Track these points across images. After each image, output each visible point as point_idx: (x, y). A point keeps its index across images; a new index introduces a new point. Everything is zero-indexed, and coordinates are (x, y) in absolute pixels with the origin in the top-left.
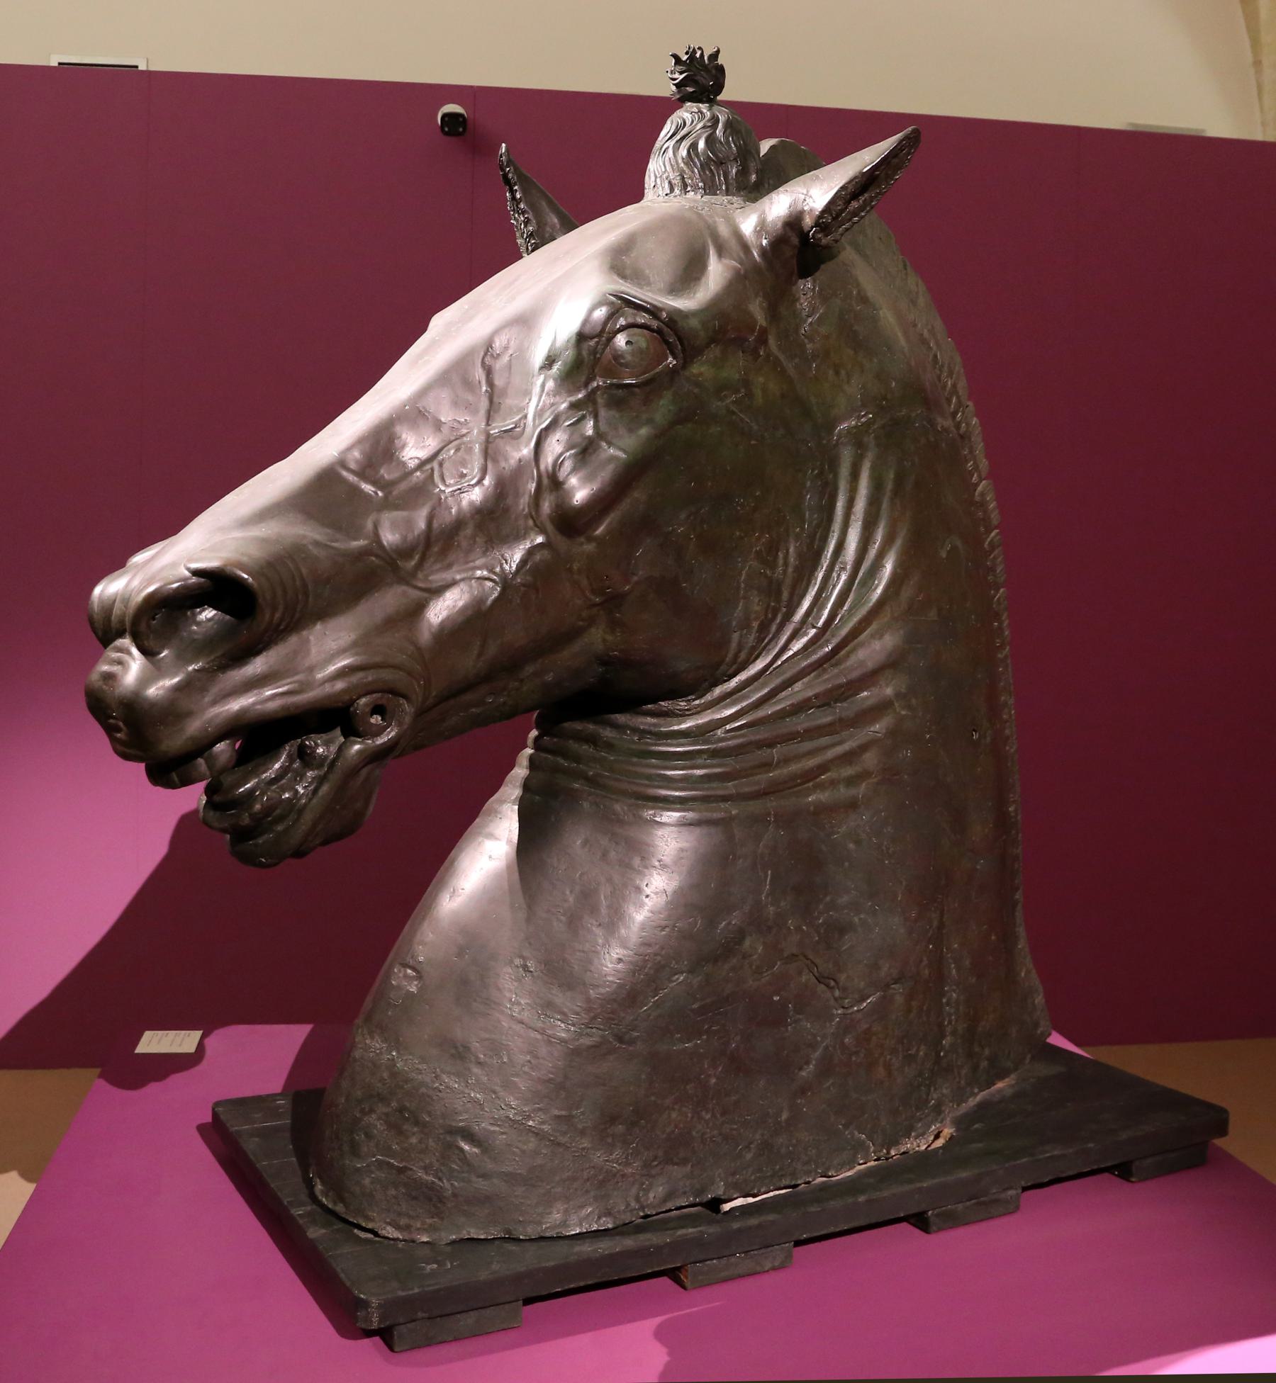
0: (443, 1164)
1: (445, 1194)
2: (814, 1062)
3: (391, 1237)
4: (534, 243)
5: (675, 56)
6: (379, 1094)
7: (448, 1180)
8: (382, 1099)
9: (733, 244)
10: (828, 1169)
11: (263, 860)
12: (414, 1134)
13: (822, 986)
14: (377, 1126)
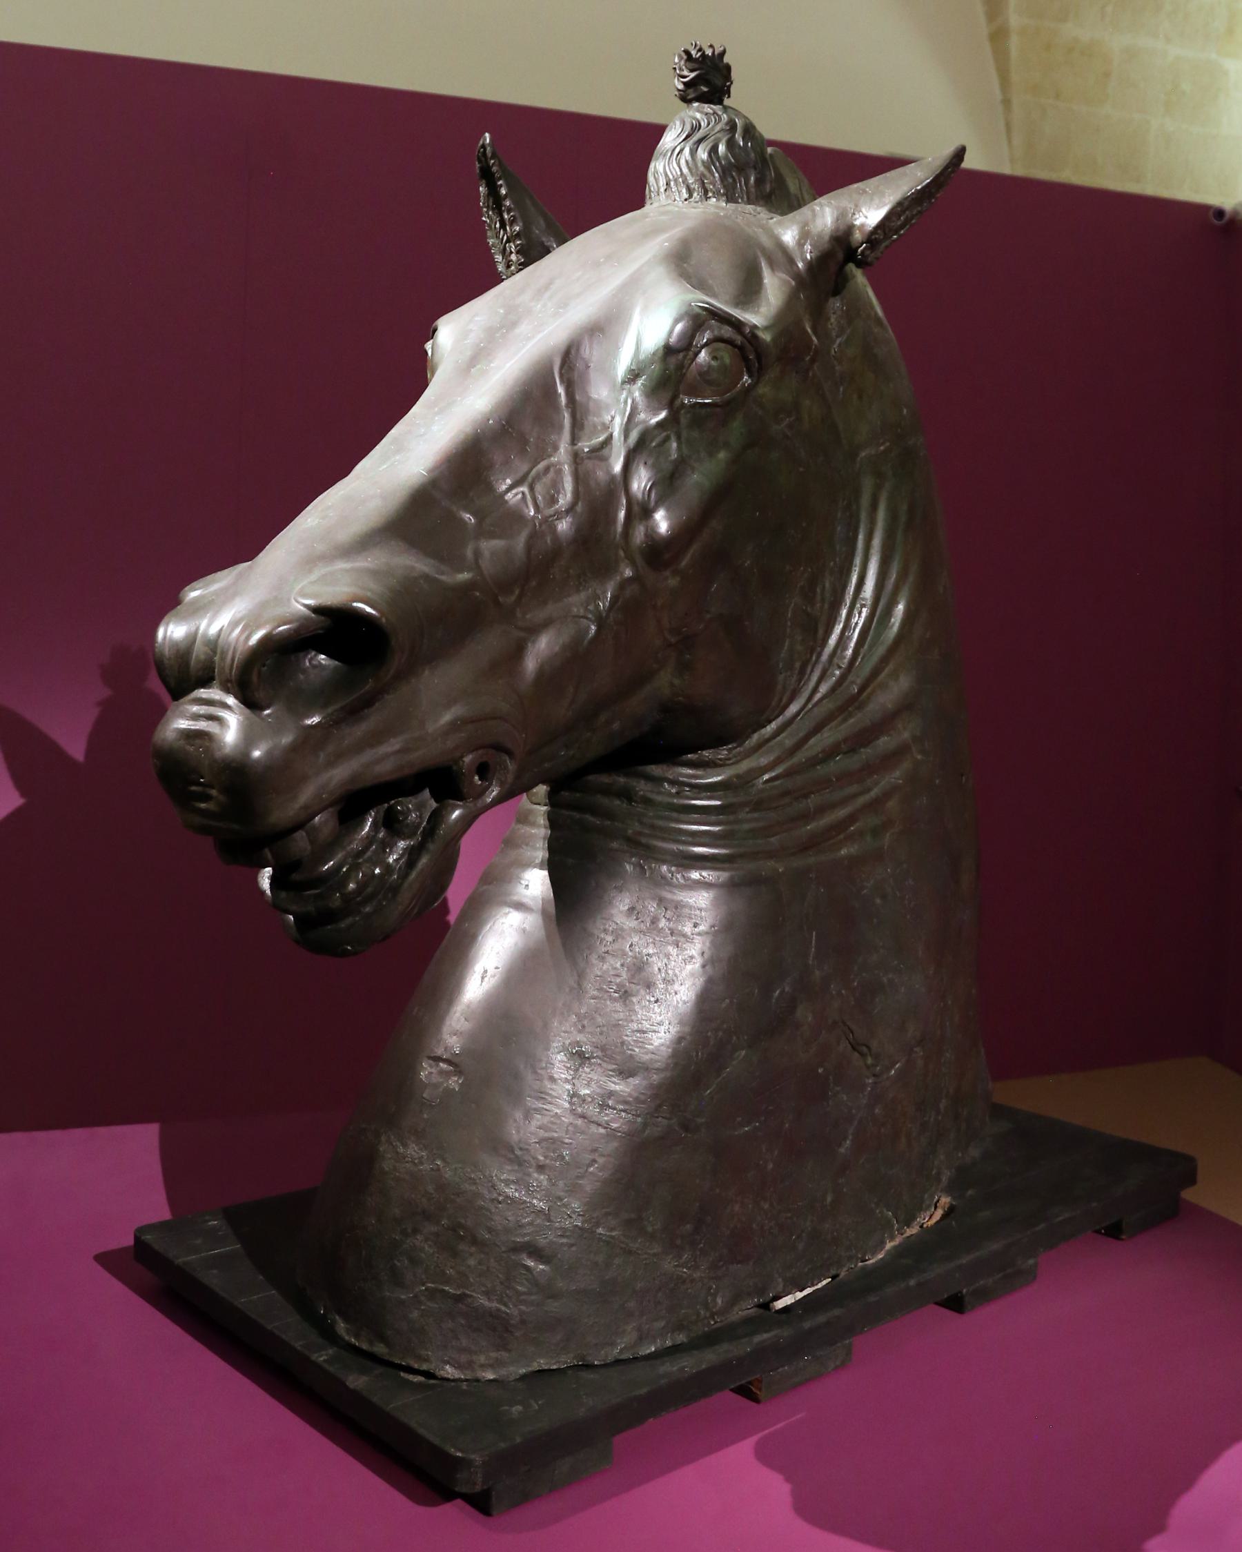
0: (509, 1288)
1: (512, 1322)
2: (850, 1137)
3: (452, 1378)
4: (520, 244)
5: (687, 52)
6: (424, 1212)
7: (515, 1306)
8: (427, 1216)
9: (779, 256)
10: (864, 1255)
11: (349, 948)
12: (471, 1255)
13: (856, 1054)
14: (424, 1248)
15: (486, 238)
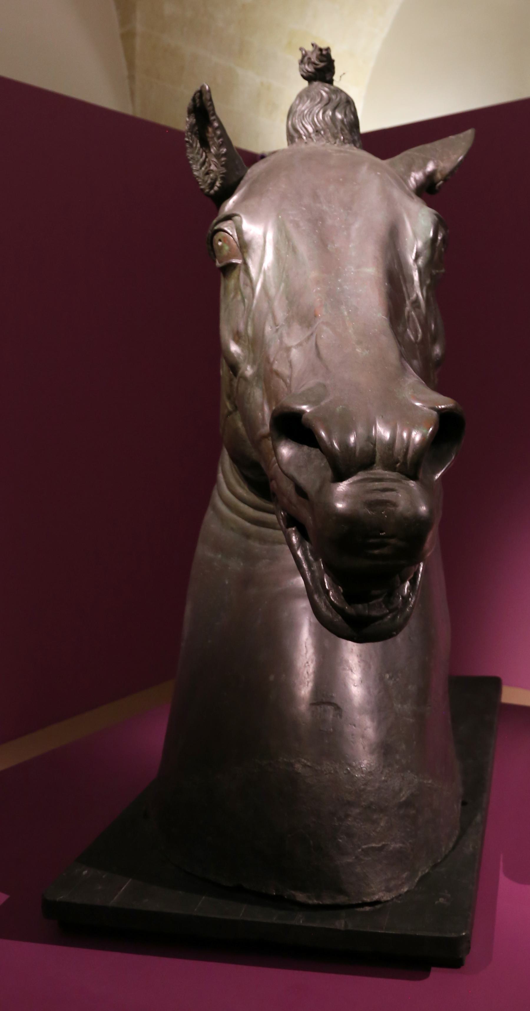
15: (191, 170)
